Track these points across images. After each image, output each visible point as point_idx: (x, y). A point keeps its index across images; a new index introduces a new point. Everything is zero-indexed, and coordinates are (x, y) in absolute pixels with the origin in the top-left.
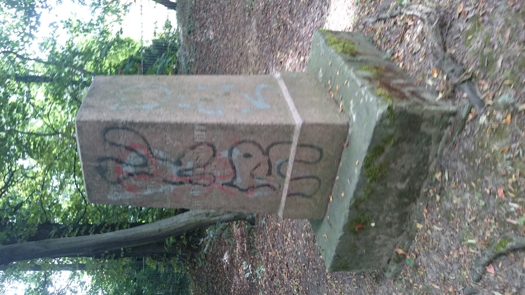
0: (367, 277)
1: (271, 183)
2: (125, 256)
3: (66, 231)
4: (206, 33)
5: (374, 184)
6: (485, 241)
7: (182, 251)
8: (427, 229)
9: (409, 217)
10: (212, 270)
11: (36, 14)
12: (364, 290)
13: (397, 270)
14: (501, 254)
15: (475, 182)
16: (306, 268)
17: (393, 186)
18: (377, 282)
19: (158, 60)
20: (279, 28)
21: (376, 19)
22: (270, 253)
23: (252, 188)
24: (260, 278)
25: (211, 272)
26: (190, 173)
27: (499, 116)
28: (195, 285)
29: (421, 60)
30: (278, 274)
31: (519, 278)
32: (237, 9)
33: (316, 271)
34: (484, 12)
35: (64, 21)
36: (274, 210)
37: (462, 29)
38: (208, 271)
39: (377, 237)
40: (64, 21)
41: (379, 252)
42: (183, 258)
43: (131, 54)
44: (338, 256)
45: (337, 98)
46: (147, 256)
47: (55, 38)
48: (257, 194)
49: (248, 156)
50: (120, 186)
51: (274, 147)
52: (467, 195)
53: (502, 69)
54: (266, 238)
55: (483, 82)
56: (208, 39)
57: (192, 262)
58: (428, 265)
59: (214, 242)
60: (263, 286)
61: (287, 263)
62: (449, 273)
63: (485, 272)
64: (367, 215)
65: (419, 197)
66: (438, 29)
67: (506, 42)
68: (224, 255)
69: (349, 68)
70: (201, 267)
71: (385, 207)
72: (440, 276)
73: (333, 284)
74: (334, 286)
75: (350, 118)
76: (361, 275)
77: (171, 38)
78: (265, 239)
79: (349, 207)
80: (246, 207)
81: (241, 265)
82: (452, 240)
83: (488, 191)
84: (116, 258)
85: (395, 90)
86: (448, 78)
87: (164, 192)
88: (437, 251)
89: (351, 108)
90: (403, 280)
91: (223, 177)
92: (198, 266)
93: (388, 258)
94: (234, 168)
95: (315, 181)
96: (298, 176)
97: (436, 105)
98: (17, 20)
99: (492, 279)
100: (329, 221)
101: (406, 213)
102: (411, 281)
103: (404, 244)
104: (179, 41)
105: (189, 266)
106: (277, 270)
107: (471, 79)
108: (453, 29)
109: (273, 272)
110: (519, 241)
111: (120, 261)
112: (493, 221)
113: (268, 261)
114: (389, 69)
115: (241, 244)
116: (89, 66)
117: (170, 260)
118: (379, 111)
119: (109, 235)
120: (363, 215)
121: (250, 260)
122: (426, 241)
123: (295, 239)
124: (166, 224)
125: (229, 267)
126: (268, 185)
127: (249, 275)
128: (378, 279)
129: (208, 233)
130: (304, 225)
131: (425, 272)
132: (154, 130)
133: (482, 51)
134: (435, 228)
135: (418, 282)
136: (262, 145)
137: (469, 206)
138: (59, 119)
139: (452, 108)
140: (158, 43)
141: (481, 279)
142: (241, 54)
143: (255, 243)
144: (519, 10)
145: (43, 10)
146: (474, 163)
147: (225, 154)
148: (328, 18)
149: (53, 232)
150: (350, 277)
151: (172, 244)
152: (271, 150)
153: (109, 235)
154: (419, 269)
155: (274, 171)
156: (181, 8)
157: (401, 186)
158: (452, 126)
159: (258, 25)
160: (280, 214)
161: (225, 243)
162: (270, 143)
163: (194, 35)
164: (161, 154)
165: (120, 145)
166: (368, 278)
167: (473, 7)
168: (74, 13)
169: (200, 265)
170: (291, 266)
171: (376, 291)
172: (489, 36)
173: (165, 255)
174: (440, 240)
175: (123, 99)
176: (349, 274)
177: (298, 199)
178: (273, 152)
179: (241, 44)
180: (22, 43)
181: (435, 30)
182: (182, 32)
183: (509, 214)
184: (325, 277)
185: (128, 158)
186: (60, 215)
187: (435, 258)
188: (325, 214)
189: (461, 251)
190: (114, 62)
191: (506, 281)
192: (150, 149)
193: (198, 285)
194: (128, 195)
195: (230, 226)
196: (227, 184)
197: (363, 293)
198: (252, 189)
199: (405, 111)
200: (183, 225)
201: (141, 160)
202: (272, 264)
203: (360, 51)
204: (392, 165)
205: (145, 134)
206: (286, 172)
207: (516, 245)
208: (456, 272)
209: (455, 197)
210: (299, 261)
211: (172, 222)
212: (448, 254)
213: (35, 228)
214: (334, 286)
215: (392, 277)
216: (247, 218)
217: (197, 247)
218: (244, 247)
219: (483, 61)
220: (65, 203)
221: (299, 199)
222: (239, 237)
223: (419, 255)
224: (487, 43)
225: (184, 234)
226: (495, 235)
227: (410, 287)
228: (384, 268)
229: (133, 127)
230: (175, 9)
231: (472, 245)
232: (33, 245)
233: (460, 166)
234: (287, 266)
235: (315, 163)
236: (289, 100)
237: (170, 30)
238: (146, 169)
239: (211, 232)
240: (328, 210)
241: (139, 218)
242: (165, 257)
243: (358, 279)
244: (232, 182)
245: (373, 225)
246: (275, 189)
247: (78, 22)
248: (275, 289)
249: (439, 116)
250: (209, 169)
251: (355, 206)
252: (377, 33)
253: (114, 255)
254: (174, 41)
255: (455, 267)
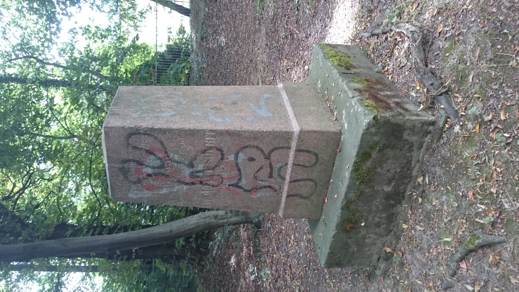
0: (361, 276)
1: (272, 185)
2: (136, 258)
3: (81, 232)
4: (218, 39)
5: (362, 187)
6: (458, 239)
7: (191, 254)
8: (411, 230)
9: (396, 218)
10: (220, 273)
11: (57, 21)
12: (358, 288)
13: (386, 267)
14: (471, 251)
15: (450, 186)
16: (307, 269)
17: (380, 189)
18: (369, 279)
19: (172, 66)
20: (286, 37)
21: (370, 35)
22: (274, 255)
23: (255, 189)
24: (265, 280)
25: (219, 275)
26: (201, 174)
27: (470, 126)
28: (203, 288)
29: (407, 73)
30: (282, 276)
31: (486, 272)
32: (248, 18)
33: (316, 271)
34: (459, 32)
35: (83, 27)
36: (275, 210)
37: (441, 47)
38: (216, 274)
39: (367, 236)
40: (83, 27)
41: (369, 250)
42: (191, 261)
43: (147, 59)
44: (332, 253)
45: (332, 107)
46: (157, 258)
47: (73, 44)
48: (259, 194)
49: (251, 159)
50: (140, 185)
52: (444, 198)
53: (473, 84)
54: (271, 241)
55: (457, 95)
56: (220, 45)
57: (200, 265)
58: (412, 262)
59: (222, 245)
60: (268, 288)
61: (290, 264)
62: (429, 269)
63: (458, 268)
64: (357, 215)
65: (404, 200)
66: (420, 46)
67: (477, 59)
68: (231, 258)
69: (342, 81)
70: (209, 270)
71: (374, 208)
72: (422, 272)
73: (331, 283)
74: (332, 284)
75: (342, 126)
76: (355, 274)
77: (184, 44)
78: (270, 242)
79: (340, 207)
80: (250, 207)
81: (247, 268)
82: (432, 238)
83: (461, 194)
84: (128, 259)
85: (381, 101)
86: (428, 91)
87: (177, 192)
88: (420, 250)
89: (344, 117)
90: (391, 277)
91: (230, 178)
92: (206, 269)
93: (378, 256)
94: (239, 170)
95: (311, 183)
96: (296, 178)
97: (418, 115)
98: (38, 26)
99: (464, 274)
100: (324, 221)
101: (393, 214)
102: (398, 278)
103: (392, 243)
104: (192, 46)
105: (197, 269)
106: (281, 272)
107: (447, 92)
108: (434, 47)
109: (277, 274)
110: (485, 238)
111: (131, 262)
112: (464, 221)
113: (273, 263)
114: (378, 82)
115: (247, 247)
116: (105, 72)
117: (179, 262)
118: (366, 120)
119: (121, 236)
120: (354, 215)
121: (256, 263)
122: (411, 241)
123: (298, 241)
124: (177, 225)
125: (236, 270)
126: (270, 187)
127: (255, 277)
128: (370, 277)
129: (216, 236)
130: (306, 227)
131: (410, 269)
132: (170, 136)
133: (458, 67)
134: (418, 228)
135: (404, 278)
136: (264, 150)
137: (445, 207)
138: (75, 123)
139: (432, 118)
140: (172, 48)
141: (455, 274)
142: (251, 61)
143: (261, 246)
144: (487, 32)
145: (64, 17)
146: (450, 168)
147: (232, 157)
148: (330, 30)
149: (69, 232)
150: (346, 276)
151: (182, 247)
152: (272, 154)
153: (121, 236)
154: (405, 266)
155: (275, 174)
156: (195, 14)
157: (388, 189)
158: (432, 135)
159: (267, 34)
160: (281, 213)
161: (233, 246)
162: (272, 148)
163: (206, 41)
164: (176, 157)
165: (141, 149)
166: (362, 276)
167: (451, 27)
168: (92, 19)
169: (208, 268)
170: (294, 267)
171: (369, 288)
172: (463, 53)
173: (174, 257)
174: (422, 240)
175: (144, 108)
176: (345, 273)
177: (296, 200)
178: (275, 156)
179: (251, 52)
180: (42, 48)
181: (418, 47)
182: (195, 38)
183: (477, 214)
184: (324, 276)
185: (148, 161)
186: (76, 216)
187: (418, 256)
188: (321, 215)
189: (439, 249)
190: (129, 67)
191: (476, 275)
192: (166, 153)
193: (206, 288)
194: (147, 194)
195: (237, 229)
196: (232, 185)
197: (357, 290)
198: (255, 190)
199: (389, 120)
200: (193, 226)
201: (158, 163)
202: (276, 266)
203: (355, 64)
204: (379, 170)
205: (163, 139)
206: (285, 175)
207: (482, 241)
208: (435, 268)
209: (434, 199)
210: (301, 262)
211: (183, 224)
212: (429, 253)
213: (52, 228)
214: (332, 284)
215: (382, 274)
216: (254, 221)
217: (205, 250)
218: (250, 250)
219: (457, 76)
220: (80, 205)
221: (298, 200)
222: (245, 240)
223: (405, 253)
224: (462, 61)
225: (194, 236)
226: (466, 233)
227: (397, 283)
228: (374, 266)
229: (153, 133)
230: (189, 16)
231: (448, 242)
232: (52, 243)
233: (439, 171)
234: (290, 267)
235: (311, 166)
236: (289, 109)
237: (183, 36)
238: (163, 171)
239: (219, 234)
240: (324, 211)
241: (150, 222)
242: (175, 260)
243: (353, 278)
244: (238, 183)
245: (363, 224)
246: (276, 191)
247: (96, 29)
248: (279, 290)
249: (420, 126)
250: (217, 171)
251: (347, 207)
252: (371, 47)
253: (126, 256)
254: (187, 47)
255: (435, 263)
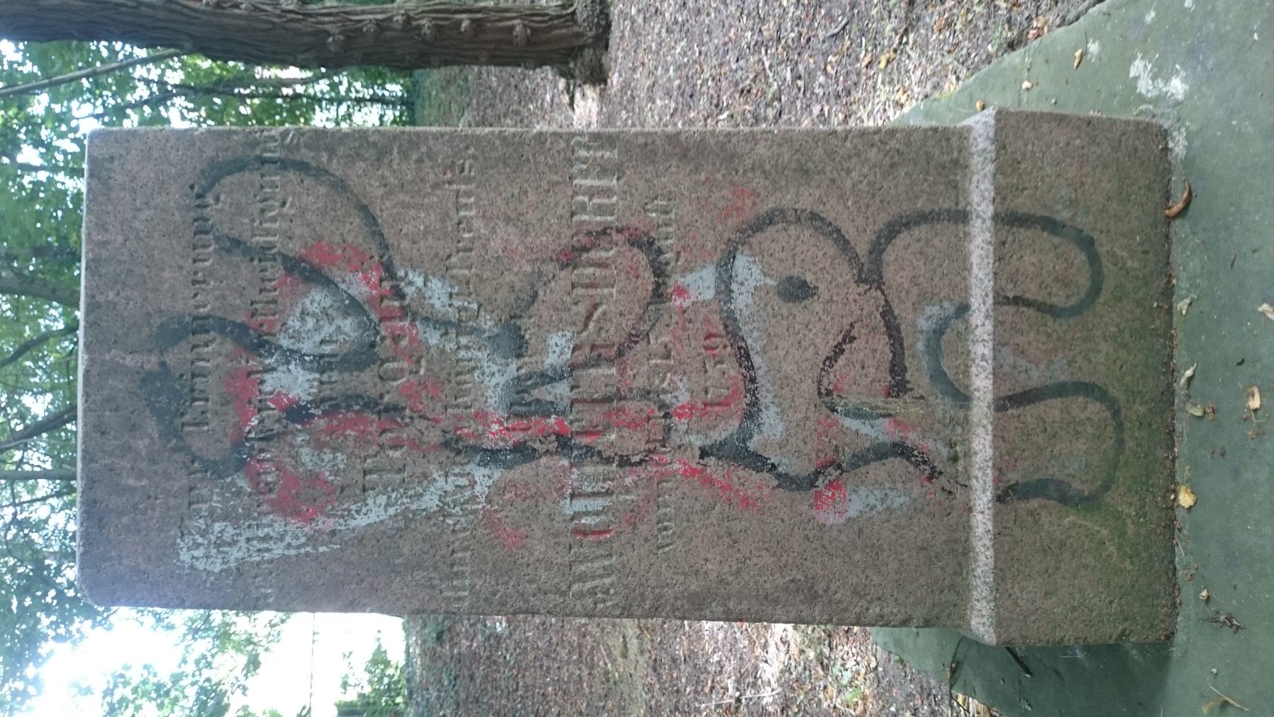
1: (912, 438)
26: (561, 390)
51: (902, 239)
87: (443, 512)
91: (708, 407)
94: (744, 356)
95: (1095, 409)
126: (901, 450)
136: (850, 233)
152: (890, 255)
155: (918, 374)
192: (389, 269)
206: (967, 373)
238: (366, 381)
246: (934, 474)
250: (640, 371)
